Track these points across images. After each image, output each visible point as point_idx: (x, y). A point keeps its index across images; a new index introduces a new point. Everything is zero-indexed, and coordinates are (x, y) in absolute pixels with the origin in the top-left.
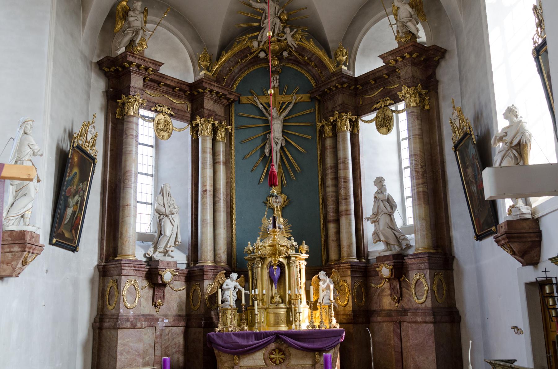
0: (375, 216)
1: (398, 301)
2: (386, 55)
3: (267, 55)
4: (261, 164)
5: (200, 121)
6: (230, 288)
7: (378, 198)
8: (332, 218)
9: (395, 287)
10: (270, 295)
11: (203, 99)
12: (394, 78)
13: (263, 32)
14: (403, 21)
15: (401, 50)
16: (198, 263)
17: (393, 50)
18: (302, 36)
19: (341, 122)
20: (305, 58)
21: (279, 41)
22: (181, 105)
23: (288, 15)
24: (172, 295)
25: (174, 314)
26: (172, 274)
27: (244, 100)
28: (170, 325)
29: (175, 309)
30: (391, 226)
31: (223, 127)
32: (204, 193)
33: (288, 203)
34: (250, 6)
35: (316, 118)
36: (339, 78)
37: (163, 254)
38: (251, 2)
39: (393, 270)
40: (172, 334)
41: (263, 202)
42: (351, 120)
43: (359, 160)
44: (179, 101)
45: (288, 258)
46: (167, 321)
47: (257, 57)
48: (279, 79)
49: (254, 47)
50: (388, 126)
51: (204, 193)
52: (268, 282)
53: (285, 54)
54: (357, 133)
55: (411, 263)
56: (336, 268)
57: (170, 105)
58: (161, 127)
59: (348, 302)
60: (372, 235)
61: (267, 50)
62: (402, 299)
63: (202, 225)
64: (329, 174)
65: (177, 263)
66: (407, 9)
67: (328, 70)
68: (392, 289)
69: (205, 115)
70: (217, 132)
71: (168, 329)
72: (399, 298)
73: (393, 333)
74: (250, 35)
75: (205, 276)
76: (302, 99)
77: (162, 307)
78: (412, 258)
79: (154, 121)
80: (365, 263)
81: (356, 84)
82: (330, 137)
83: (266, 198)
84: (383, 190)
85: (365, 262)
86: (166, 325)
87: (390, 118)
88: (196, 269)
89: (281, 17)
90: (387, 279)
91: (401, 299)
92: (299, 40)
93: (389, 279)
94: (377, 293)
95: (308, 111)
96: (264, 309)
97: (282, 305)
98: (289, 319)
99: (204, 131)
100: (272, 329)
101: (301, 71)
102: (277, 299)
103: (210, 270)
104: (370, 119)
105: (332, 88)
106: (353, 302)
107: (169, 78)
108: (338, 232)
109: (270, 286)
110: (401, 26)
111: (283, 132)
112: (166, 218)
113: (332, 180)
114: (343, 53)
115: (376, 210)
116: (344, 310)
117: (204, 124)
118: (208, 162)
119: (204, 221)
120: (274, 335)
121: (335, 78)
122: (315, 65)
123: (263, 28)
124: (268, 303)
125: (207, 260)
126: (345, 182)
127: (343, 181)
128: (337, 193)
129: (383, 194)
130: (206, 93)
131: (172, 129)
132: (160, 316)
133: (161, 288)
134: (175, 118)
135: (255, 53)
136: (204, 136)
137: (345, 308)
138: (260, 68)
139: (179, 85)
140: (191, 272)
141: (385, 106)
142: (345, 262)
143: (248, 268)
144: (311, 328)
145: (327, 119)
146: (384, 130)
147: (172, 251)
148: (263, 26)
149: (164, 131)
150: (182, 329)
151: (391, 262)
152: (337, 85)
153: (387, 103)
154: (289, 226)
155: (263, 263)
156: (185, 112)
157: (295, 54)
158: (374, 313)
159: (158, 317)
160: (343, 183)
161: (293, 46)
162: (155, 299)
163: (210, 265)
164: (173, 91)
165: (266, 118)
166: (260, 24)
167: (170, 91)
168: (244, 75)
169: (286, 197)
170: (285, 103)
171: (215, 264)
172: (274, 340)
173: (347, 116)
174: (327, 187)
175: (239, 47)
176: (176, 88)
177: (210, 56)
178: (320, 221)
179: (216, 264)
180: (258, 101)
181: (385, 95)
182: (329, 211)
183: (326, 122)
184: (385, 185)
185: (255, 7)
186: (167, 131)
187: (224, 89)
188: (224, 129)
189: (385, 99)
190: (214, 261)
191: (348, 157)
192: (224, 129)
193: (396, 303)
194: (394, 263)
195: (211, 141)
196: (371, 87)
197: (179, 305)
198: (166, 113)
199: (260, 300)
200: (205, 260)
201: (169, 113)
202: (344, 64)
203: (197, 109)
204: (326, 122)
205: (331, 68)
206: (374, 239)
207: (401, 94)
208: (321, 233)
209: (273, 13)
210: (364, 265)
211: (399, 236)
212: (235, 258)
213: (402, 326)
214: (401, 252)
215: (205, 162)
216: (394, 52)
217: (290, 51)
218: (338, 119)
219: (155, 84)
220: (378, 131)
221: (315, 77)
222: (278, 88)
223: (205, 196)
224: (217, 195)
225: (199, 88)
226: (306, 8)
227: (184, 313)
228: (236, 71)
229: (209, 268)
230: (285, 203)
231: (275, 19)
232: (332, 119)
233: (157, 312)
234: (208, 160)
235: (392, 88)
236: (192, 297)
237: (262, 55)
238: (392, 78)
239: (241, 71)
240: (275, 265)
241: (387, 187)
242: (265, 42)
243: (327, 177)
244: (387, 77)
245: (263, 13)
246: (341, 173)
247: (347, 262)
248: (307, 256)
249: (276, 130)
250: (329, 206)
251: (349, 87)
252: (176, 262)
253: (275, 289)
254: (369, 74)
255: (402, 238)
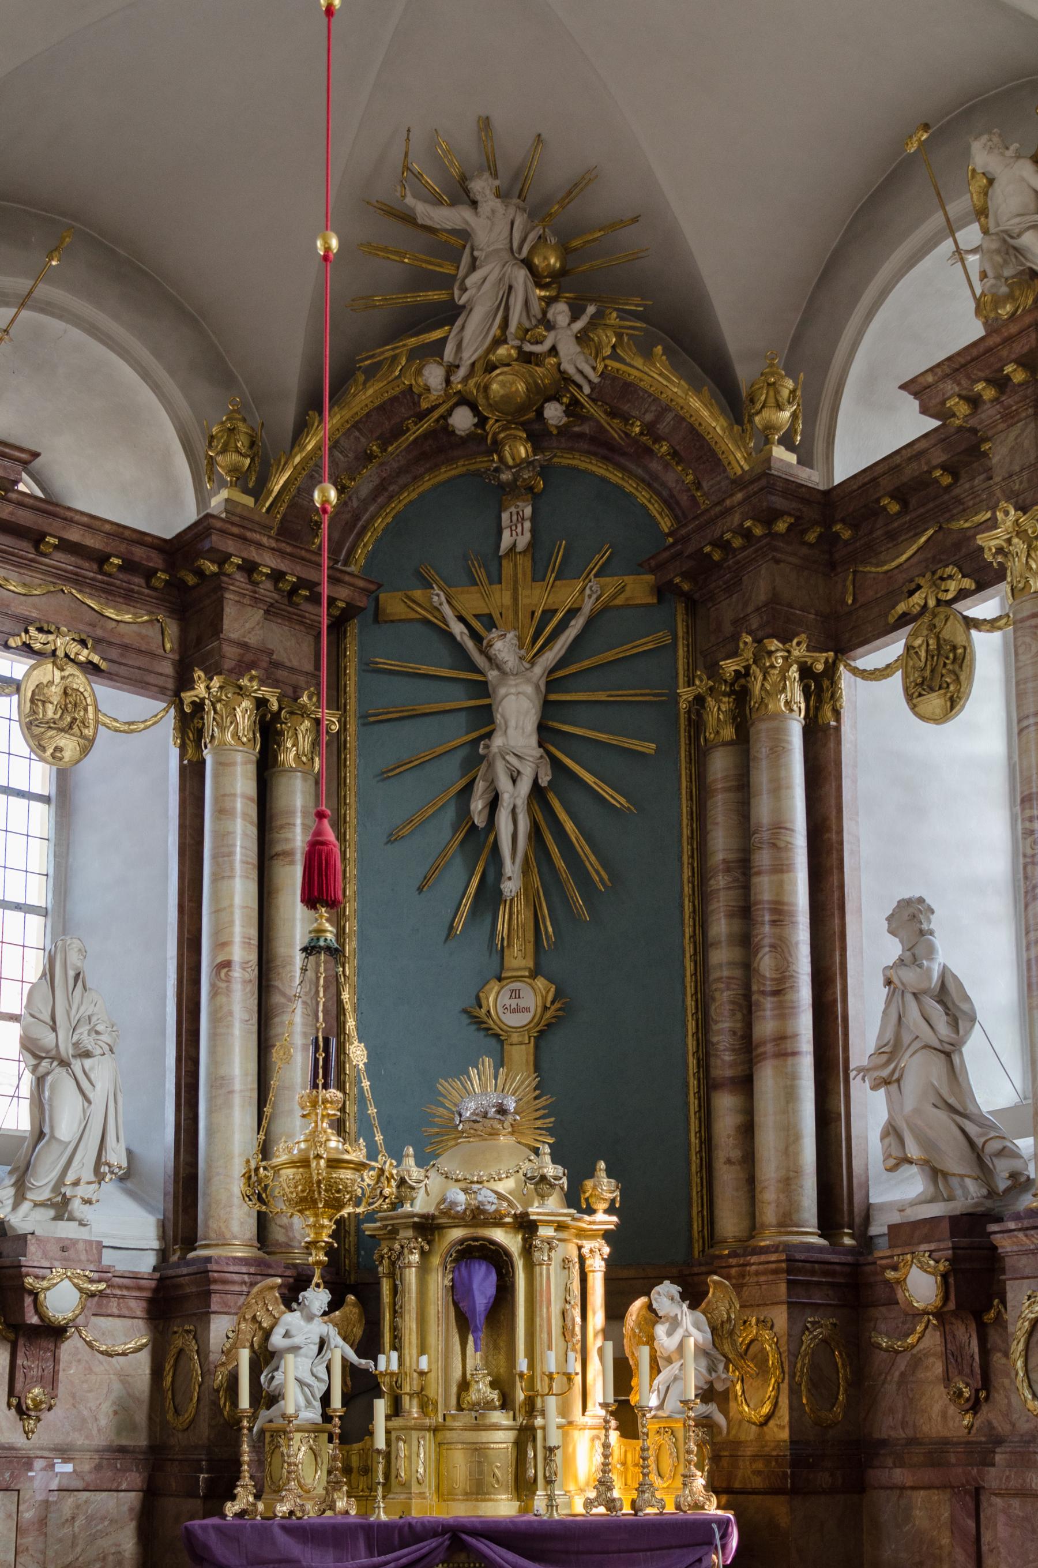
0: (885, 1057)
1: (975, 1407)
2: (930, 379)
3: (482, 421)
4: (458, 862)
5: (208, 688)
6: (299, 1348)
7: (899, 985)
8: (728, 1073)
9: (961, 1348)
10: (457, 1374)
11: (220, 601)
12: (976, 482)
13: (463, 328)
14: (1005, 232)
15: (989, 350)
16: (195, 1249)
17: (959, 354)
18: (619, 336)
19: (765, 679)
20: (632, 425)
21: (527, 358)
22: (134, 627)
23: (566, 251)
24: (90, 1370)
25: (100, 1440)
26: (81, 1290)
27: (394, 605)
28: (79, 1484)
29: (103, 1422)
30: (951, 1100)
31: (304, 713)
32: (218, 973)
33: (560, 1013)
34: (408, 218)
35: (677, 669)
36: (755, 493)
37: (52, 1213)
38: (410, 200)
39: (951, 1280)
40: (90, 1519)
41: (465, 1011)
42: (806, 672)
43: (840, 832)
44: (128, 613)
45: (526, 1226)
46: (69, 1468)
47: (444, 429)
48: (533, 519)
49: (428, 390)
50: (952, 688)
51: (218, 973)
52: (447, 1325)
53: (554, 413)
54: (833, 723)
55: (1015, 1248)
56: (733, 1271)
57: (88, 629)
58: (50, 714)
59: (775, 1405)
60: (882, 1139)
61: (481, 401)
62: (987, 1398)
63: (210, 1099)
64: (722, 893)
65: (100, 1246)
66: (1023, 179)
67: (725, 470)
68: (953, 1357)
69: (228, 664)
70: (281, 733)
71: (70, 1500)
72: (977, 1391)
73: (948, 1534)
74: (413, 341)
75: (215, 1299)
76: (623, 596)
77: (46, 1416)
78: (1020, 1230)
79: (18, 690)
80: (850, 1250)
81: (827, 522)
82: (725, 744)
83: (475, 993)
84: (919, 951)
85: (852, 1247)
86: (65, 1486)
87: (960, 651)
88: (184, 1271)
89: (536, 261)
90: (934, 1314)
91: (983, 1395)
92: (608, 351)
93: (939, 1314)
94: (897, 1374)
95: (646, 644)
96: (429, 1430)
97: (499, 1417)
98: (525, 1471)
99: (223, 729)
100: (459, 1511)
101: (620, 482)
102: (482, 1389)
103: (236, 1277)
104: (881, 665)
105: (728, 541)
106: (794, 1408)
107: (77, 517)
108: (748, 1130)
109: (456, 1339)
110: (998, 251)
111: (545, 732)
112: (60, 1072)
113: (730, 915)
114: (777, 392)
115: (889, 1035)
116: (760, 1436)
117: (220, 700)
118: (238, 849)
119: (219, 1082)
120: (443, 1533)
121: (739, 496)
122: (675, 454)
123: (463, 307)
124: (447, 1406)
125: (228, 1236)
126: (774, 923)
127: (767, 918)
128: (747, 967)
129: (920, 966)
130: (228, 576)
131: (97, 722)
132: (42, 1449)
133: (44, 1344)
134: (111, 679)
135: (436, 415)
136: (221, 749)
137: (765, 1428)
138: (460, 476)
139: (123, 548)
140: (168, 1282)
141: (939, 602)
142: (767, 1247)
143: (380, 1269)
144: (602, 1510)
145: (713, 670)
146: (935, 701)
147: (88, 1202)
148: (461, 302)
149: (62, 730)
150: (131, 1499)
151: (942, 1245)
152: (748, 524)
153: (947, 591)
154: (543, 1102)
155: (427, 1247)
156: (152, 655)
157: (592, 409)
158: (882, 1452)
159: (32, 1454)
160: (767, 929)
161: (586, 377)
162: (18, 1386)
163: (239, 1254)
164: (101, 571)
165: (480, 678)
166: (453, 294)
167: (89, 569)
168: (397, 506)
169: (553, 990)
170: (555, 612)
171: (260, 1254)
172: (441, 1556)
173: (789, 652)
174: (712, 944)
175: (370, 392)
176: (108, 557)
177: (253, 429)
178: (687, 1085)
179: (268, 1253)
180: (447, 610)
181: (943, 557)
182: (718, 1043)
183: (711, 683)
184: (931, 933)
185: (429, 223)
186: (76, 730)
187: (303, 559)
188: (307, 723)
189: (939, 573)
190: (259, 1241)
191: (792, 821)
192: (307, 723)
193: (967, 1411)
194: (953, 1248)
195: (252, 769)
196: (890, 528)
197: (122, 1411)
198: (72, 660)
199: (411, 1396)
200: (221, 1235)
201: (82, 658)
202: (780, 442)
203: (199, 642)
204: (711, 683)
205: (734, 463)
206: (887, 1156)
207: (993, 543)
208: (689, 1131)
209: (502, 244)
210: (849, 1259)
211: (983, 1140)
212: (352, 1232)
213: (984, 1504)
214: (989, 1203)
215: (225, 850)
216: (962, 361)
217: (575, 402)
218: (754, 667)
219: (25, 545)
220: (913, 708)
221: (677, 503)
222: (529, 556)
223: (223, 985)
224: (276, 983)
225: (200, 555)
226: (635, 220)
227: (143, 1441)
228: (364, 491)
229: (231, 1269)
230: (548, 1015)
231: (508, 268)
232: (730, 667)
233: (26, 1433)
234: (238, 843)
235: (967, 525)
236: (169, 1379)
237: (462, 420)
238: (967, 486)
239: (385, 489)
240: (316, 1248)
241: (939, 941)
242: (473, 364)
243: (711, 908)
244: (947, 480)
245: (464, 247)
246: (764, 887)
247: (775, 1249)
248: (610, 1221)
249: (512, 723)
250: (716, 1022)
251: (797, 529)
252: (99, 1243)
253: (476, 1350)
254: (879, 470)
255: (994, 1146)
